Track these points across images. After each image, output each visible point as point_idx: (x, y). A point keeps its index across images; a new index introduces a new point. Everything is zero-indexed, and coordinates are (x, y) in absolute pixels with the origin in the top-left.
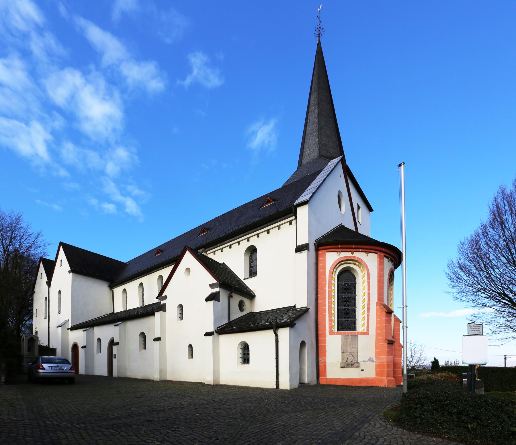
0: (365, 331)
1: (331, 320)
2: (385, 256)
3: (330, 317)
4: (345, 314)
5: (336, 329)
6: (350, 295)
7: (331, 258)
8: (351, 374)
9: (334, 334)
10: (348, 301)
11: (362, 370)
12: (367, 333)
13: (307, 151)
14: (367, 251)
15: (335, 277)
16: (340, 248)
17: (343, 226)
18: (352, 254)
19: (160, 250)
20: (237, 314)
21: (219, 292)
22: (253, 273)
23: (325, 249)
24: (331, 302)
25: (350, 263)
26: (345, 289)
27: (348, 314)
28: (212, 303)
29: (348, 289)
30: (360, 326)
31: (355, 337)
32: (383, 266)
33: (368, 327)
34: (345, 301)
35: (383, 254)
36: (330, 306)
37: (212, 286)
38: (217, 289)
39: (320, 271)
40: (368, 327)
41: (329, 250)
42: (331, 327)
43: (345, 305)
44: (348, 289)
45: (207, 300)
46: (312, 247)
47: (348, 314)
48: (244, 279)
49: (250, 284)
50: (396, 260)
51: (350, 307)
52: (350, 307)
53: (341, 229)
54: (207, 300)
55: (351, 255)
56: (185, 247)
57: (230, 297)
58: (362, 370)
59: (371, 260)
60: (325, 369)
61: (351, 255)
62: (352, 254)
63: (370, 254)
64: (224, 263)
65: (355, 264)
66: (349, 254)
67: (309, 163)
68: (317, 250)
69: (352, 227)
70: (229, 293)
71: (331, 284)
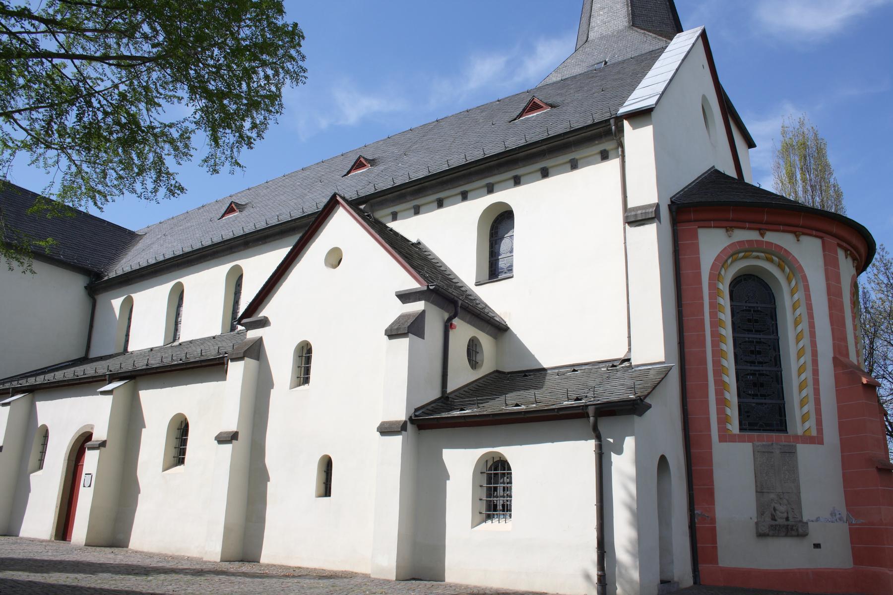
0: (814, 433)
1: (722, 402)
2: (839, 245)
3: (720, 393)
4: (755, 385)
5: (734, 427)
6: (761, 336)
7: (712, 244)
8: (784, 556)
9: (732, 438)
10: (759, 353)
11: (817, 546)
12: (818, 440)
13: (599, 15)
14: (798, 231)
15: (724, 287)
16: (733, 220)
17: (717, 171)
18: (762, 235)
19: (237, 205)
20: (462, 375)
21: (424, 311)
22: (494, 270)
23: (695, 221)
24: (718, 354)
25: (758, 257)
26: (749, 320)
27: (762, 385)
28: (403, 344)
29: (756, 321)
30: (799, 417)
31: (790, 453)
32: (839, 269)
33: (819, 422)
34: (752, 352)
35: (834, 241)
36: (717, 364)
37: (405, 297)
38: (418, 306)
39: (686, 272)
40: (819, 422)
41: (706, 223)
42: (723, 420)
43: (752, 363)
44: (756, 321)
45: (393, 333)
46: (665, 213)
47: (762, 385)
48: (478, 284)
49: (494, 297)
50: (860, 255)
51: (765, 368)
52: (765, 368)
53: (714, 177)
54: (393, 333)
55: (760, 238)
56: (334, 195)
57: (448, 327)
58: (817, 546)
59: (808, 252)
60: (714, 541)
61: (760, 238)
62: (762, 235)
63: (804, 238)
64: (419, 243)
65: (771, 261)
66: (752, 235)
67: (602, 38)
68: (675, 222)
69: (732, 173)
70: (446, 316)
71: (715, 307)
